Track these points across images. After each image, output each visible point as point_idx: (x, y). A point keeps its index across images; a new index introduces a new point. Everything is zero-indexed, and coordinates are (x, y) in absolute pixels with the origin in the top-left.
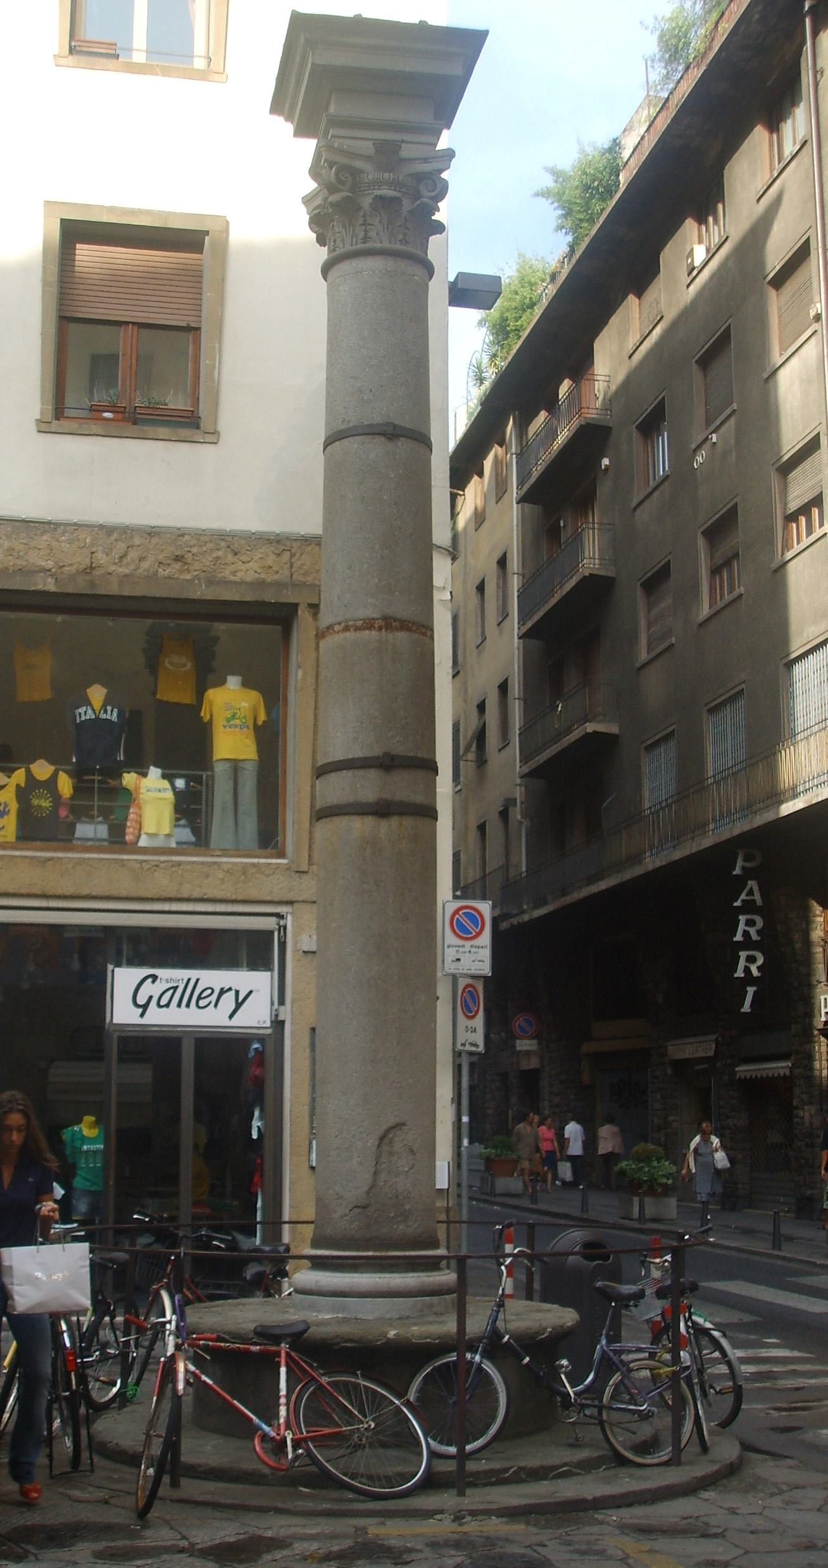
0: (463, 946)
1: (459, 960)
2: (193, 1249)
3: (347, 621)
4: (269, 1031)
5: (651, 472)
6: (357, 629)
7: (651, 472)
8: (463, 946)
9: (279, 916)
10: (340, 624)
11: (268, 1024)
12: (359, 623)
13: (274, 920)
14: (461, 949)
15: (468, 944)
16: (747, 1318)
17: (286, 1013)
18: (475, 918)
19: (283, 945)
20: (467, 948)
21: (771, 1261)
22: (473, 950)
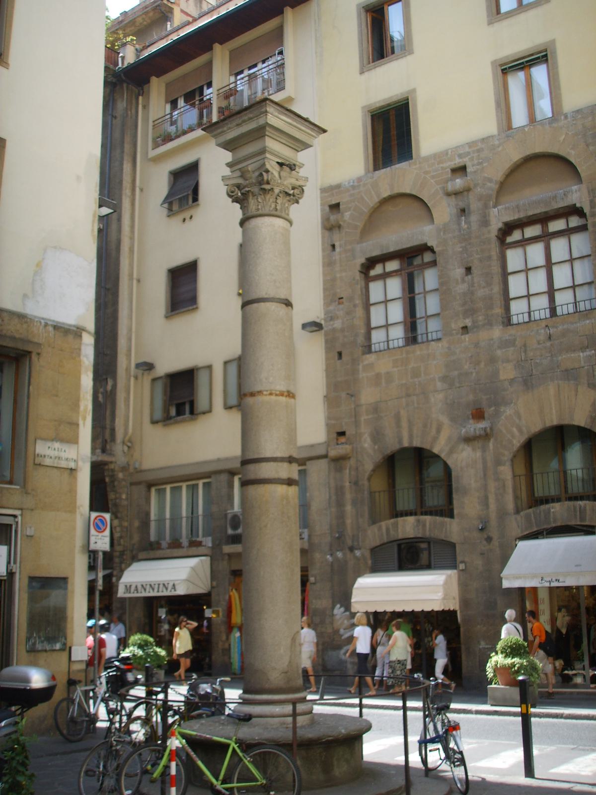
0: (98, 536)
1: (96, 543)
2: (279, 755)
3: (271, 390)
4: (5, 578)
5: (160, 120)
6: (276, 395)
7: (160, 120)
8: (98, 536)
9: (15, 516)
10: (267, 391)
11: (5, 574)
12: (278, 392)
13: (12, 518)
14: (97, 537)
15: (100, 534)
16: (424, 757)
17: (16, 568)
18: (103, 521)
19: (16, 531)
20: (100, 537)
21: (6, 606)
22: (103, 538)
